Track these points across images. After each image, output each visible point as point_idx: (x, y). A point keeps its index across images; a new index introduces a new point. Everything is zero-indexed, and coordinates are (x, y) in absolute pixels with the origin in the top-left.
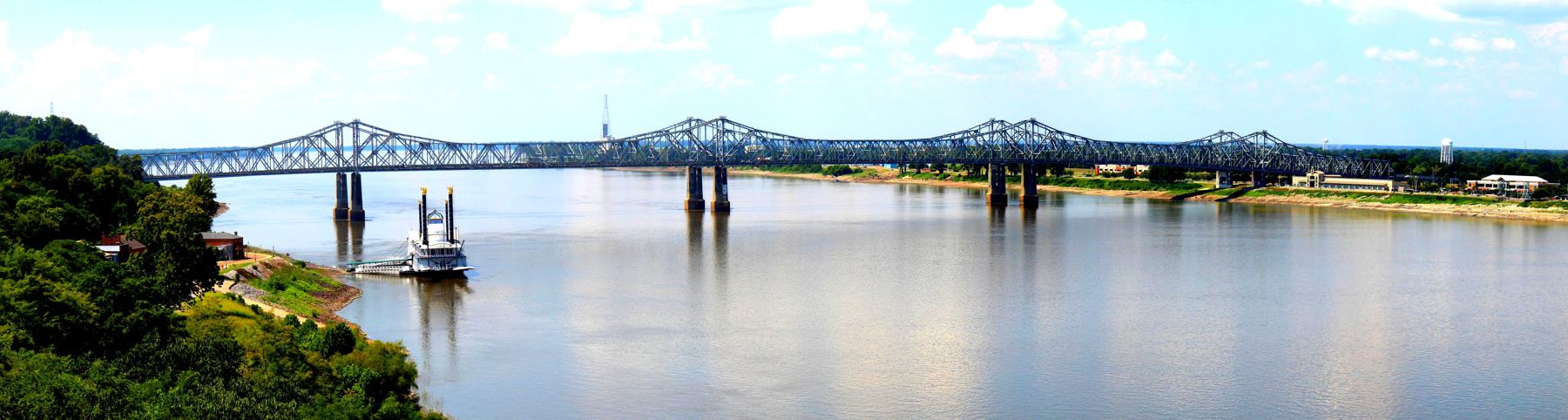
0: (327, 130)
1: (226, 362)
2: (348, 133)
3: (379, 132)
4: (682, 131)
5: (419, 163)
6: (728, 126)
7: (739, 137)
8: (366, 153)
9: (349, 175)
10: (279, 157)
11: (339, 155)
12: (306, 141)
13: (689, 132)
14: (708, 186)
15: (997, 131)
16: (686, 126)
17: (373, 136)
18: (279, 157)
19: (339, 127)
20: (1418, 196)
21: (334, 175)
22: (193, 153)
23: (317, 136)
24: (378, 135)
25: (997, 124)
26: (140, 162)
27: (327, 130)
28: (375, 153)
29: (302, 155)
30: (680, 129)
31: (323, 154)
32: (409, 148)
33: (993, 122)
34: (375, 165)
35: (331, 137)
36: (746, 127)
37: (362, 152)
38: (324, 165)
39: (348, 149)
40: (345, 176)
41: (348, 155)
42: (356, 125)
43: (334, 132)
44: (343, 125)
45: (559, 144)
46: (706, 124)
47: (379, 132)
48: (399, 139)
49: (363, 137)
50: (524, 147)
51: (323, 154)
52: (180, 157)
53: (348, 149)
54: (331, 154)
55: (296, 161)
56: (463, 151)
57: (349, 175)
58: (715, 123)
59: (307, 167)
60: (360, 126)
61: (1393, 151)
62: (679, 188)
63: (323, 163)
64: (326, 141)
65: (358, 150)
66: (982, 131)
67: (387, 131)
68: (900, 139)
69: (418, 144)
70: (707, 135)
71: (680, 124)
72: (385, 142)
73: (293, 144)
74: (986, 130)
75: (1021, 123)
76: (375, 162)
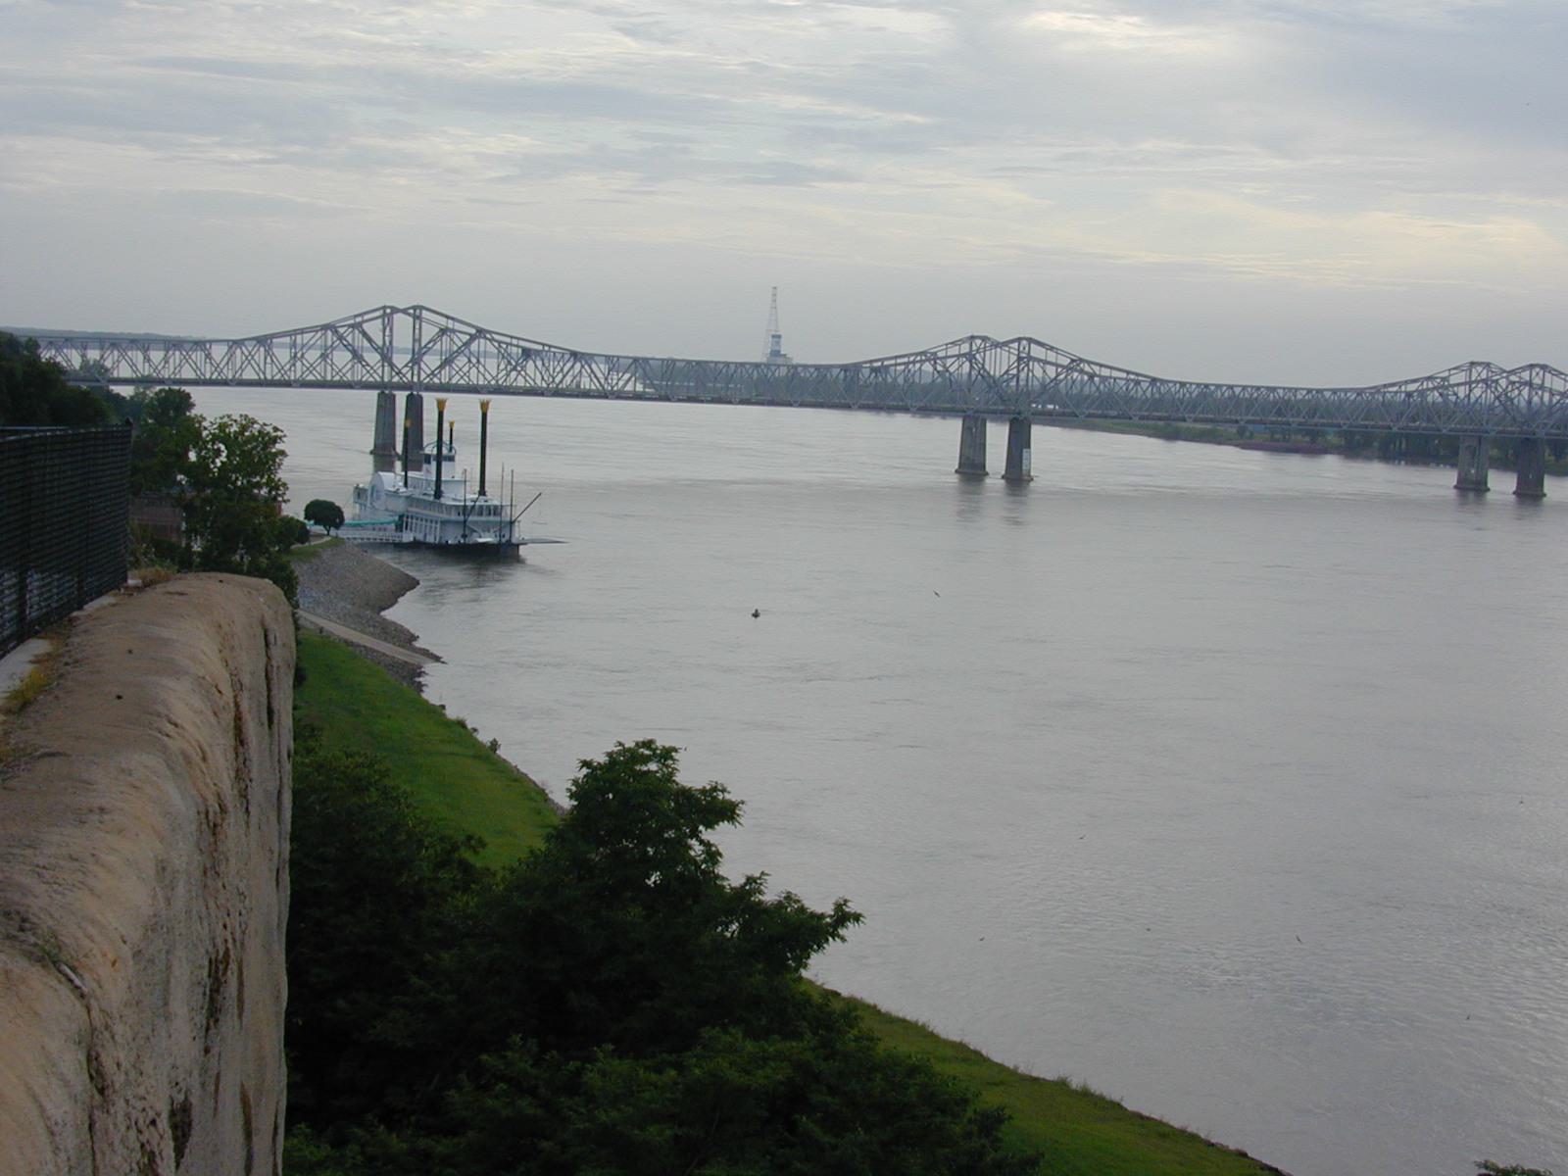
0: (366, 317)
1: (600, 800)
2: (403, 323)
3: (458, 326)
4: (958, 356)
5: (521, 382)
6: (1037, 352)
7: (1051, 371)
8: (431, 361)
9: (401, 398)
10: (283, 355)
11: (386, 357)
12: (329, 333)
13: (970, 357)
14: (997, 436)
15: (1477, 382)
16: (965, 348)
17: (443, 331)
18: (283, 355)
19: (388, 314)
20: (488, 522)
21: (373, 395)
22: (67, 340)
23: (350, 326)
24: (453, 331)
25: (1479, 369)
26: (37, 346)
27: (366, 317)
28: (447, 362)
29: (324, 356)
30: (954, 351)
31: (357, 356)
32: (503, 355)
33: (973, 338)
34: (386, 380)
35: (374, 329)
36: (1065, 354)
37: (425, 358)
38: (299, 374)
39: (404, 351)
40: (394, 397)
41: (401, 360)
42: (416, 313)
43: (380, 321)
44: (395, 310)
45: (698, 363)
46: (997, 345)
47: (458, 326)
48: (492, 340)
49: (429, 332)
50: (638, 364)
51: (357, 356)
52: (107, 345)
53: (404, 351)
54: (372, 358)
55: (311, 368)
56: (594, 366)
57: (401, 398)
58: (1016, 345)
59: (329, 378)
60: (425, 314)
61: (11, 335)
62: (948, 432)
63: (360, 374)
64: (364, 334)
65: (416, 360)
66: (1453, 380)
67: (473, 326)
68: (723, 360)
69: (520, 351)
70: (999, 364)
71: (953, 343)
72: (467, 344)
73: (307, 336)
74: (1460, 377)
75: (1523, 369)
76: (444, 377)
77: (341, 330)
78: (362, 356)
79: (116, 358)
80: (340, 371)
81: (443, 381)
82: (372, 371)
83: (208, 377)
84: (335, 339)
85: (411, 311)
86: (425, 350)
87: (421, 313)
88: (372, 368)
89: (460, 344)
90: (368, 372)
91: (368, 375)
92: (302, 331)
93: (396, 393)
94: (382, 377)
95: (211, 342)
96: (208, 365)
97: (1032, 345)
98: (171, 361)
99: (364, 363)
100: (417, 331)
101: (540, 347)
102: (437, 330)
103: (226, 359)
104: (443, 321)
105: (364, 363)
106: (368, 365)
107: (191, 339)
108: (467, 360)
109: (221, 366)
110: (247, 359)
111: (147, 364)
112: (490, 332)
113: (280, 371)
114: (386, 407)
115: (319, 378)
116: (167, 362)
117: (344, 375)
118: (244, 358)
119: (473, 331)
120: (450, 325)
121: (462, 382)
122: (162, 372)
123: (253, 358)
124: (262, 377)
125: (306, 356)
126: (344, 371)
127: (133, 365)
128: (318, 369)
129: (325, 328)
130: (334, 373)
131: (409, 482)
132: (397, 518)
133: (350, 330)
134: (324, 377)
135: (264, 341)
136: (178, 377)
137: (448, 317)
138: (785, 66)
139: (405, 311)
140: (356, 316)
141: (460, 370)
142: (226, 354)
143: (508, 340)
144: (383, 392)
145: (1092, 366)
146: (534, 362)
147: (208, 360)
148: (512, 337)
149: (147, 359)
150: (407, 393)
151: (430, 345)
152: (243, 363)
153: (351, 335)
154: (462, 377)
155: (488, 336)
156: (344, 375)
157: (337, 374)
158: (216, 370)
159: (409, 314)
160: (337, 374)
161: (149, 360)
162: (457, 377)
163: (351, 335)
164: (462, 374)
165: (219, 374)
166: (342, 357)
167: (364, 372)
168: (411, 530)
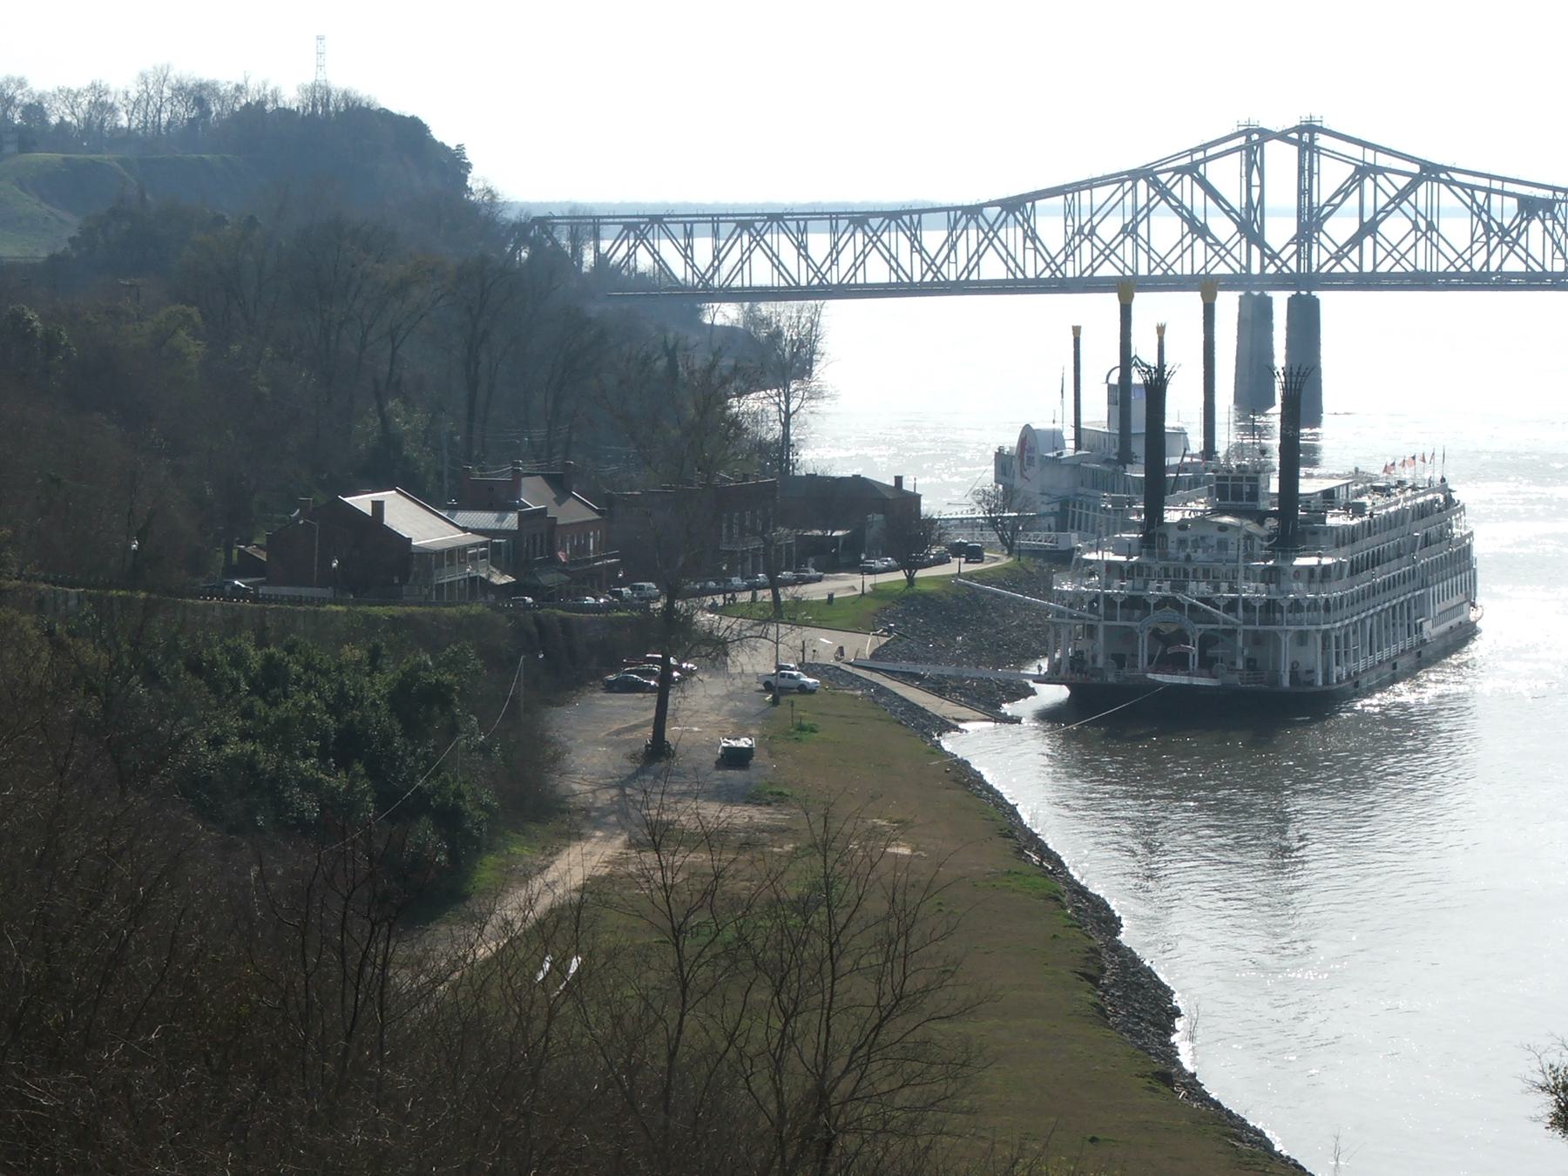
0: (1211, 152)
2: (1281, 160)
5: (1514, 265)
8: (1340, 227)
9: (1280, 301)
12: (1142, 184)
17: (1364, 171)
19: (1252, 142)
23: (1177, 170)
24: (1381, 170)
27: (1211, 152)
28: (1368, 228)
35: (1226, 174)
41: (1280, 230)
42: (1306, 138)
44: (1266, 135)
47: (1383, 160)
48: (1450, 183)
49: (1332, 175)
51: (1199, 230)
54: (1222, 227)
55: (1108, 252)
57: (1280, 301)
59: (1143, 271)
60: (1322, 141)
72: (1403, 195)
73: (1101, 194)
76: (1368, 258)
77: (1163, 178)
78: (1205, 226)
79: (859, 248)
80: (1163, 260)
81: (1418, 268)
82: (1223, 253)
83: (917, 278)
84: (1152, 193)
85: (1295, 136)
86: (1327, 209)
87: (1312, 139)
88: (1223, 247)
89: (1393, 193)
90: (1217, 253)
91: (1217, 259)
92: (1091, 184)
93: (1320, 295)
94: (1360, 267)
95: (921, 212)
96: (1030, 254)
97: (875, 228)
98: (961, 244)
99: (1210, 240)
100: (611, 220)
101: (1549, 194)
102: (1351, 169)
103: (945, 250)
104: (1356, 151)
105: (1210, 240)
106: (1218, 243)
107: (878, 209)
108: (1410, 226)
109: (938, 262)
110: (986, 236)
111: (916, 256)
112: (1445, 169)
113: (1048, 266)
114: (1255, 321)
115: (1237, 268)
116: (953, 247)
117: (1170, 267)
118: (867, 240)
119: (1415, 169)
120: (1370, 157)
121: (1398, 269)
122: (944, 269)
123: (996, 235)
124: (1020, 276)
125: (1097, 232)
126: (1102, 257)
127: (892, 260)
128: (1235, 252)
129: (1135, 175)
130: (1153, 265)
131: (1083, 440)
132: (1057, 508)
133: (1178, 176)
134: (911, 279)
135: (1015, 206)
136: (974, 277)
137: (1365, 145)
138: (83, 156)
139: (1283, 136)
140: (1193, 151)
141: (1395, 248)
142: (947, 240)
143: (1484, 182)
144: (1248, 294)
145: (1004, 242)
146: (1543, 221)
147: (1029, 244)
148: (1491, 177)
149: (802, 247)
150: (1288, 294)
151: (1337, 201)
152: (979, 245)
153: (1151, 196)
154: (1398, 262)
155: (1443, 176)
156: (1170, 267)
157: (1158, 265)
158: (929, 268)
159: (1291, 141)
160: (1158, 265)
161: (921, 250)
162: (1390, 262)
163: (1151, 196)
164: (1395, 253)
165: (935, 275)
166: (1165, 229)
167: (1210, 253)
168: (1079, 529)
